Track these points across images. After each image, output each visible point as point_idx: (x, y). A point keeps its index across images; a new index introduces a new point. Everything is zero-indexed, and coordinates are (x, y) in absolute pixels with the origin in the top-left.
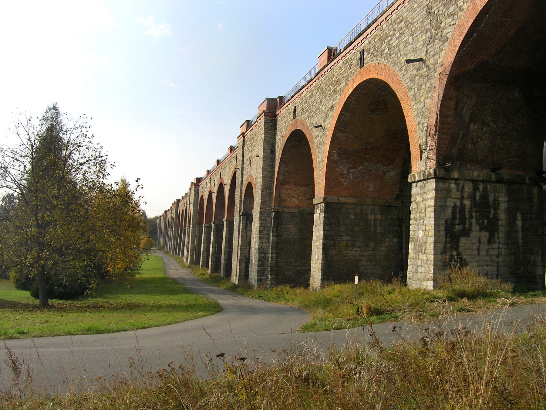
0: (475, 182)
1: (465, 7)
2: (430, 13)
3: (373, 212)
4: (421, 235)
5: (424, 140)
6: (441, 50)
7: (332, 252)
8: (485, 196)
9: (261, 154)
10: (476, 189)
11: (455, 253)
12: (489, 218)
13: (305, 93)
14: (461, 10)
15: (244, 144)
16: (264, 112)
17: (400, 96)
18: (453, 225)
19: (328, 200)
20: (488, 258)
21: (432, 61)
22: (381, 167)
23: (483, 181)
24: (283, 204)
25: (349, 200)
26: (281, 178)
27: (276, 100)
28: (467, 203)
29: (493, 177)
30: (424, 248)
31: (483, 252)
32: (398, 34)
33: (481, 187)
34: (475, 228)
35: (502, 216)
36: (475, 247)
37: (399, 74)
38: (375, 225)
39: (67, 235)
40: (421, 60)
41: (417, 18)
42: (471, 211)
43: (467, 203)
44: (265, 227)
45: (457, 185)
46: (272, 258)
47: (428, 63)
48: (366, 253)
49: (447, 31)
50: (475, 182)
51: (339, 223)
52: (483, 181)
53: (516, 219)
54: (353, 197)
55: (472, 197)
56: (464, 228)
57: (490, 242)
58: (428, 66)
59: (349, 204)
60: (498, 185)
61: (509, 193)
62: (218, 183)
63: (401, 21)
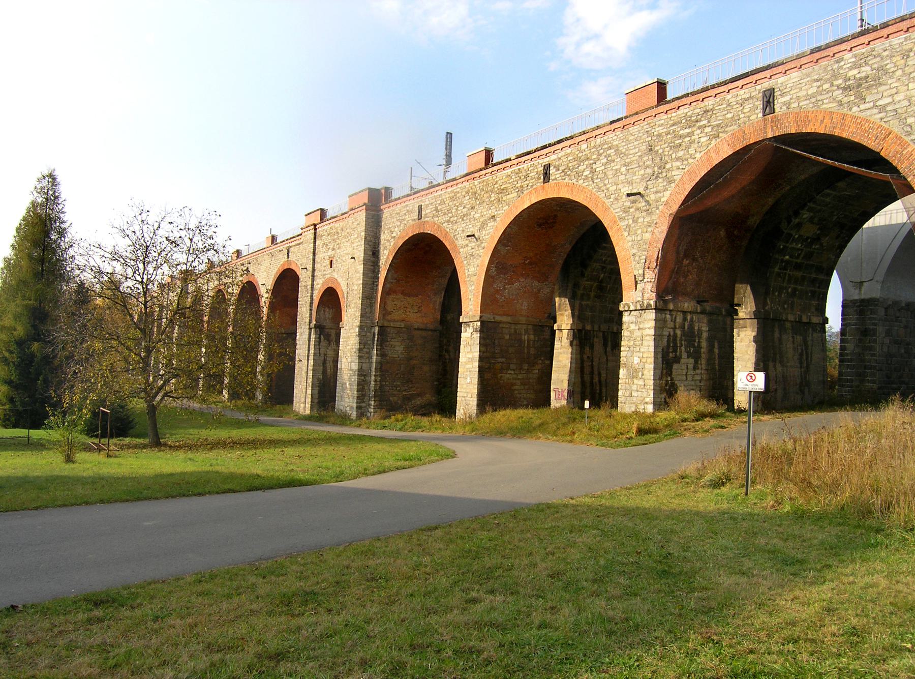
1: (698, 156)
2: (651, 150)
4: (636, 362)
5: (641, 272)
8: (691, 327)
10: (685, 319)
15: (315, 238)
16: (365, 204)
18: (668, 353)
19: (484, 319)
20: (693, 383)
21: (653, 197)
22: (536, 283)
23: (690, 312)
24: (389, 317)
25: (505, 319)
26: (388, 286)
27: (378, 190)
28: (679, 332)
30: (640, 374)
31: (689, 378)
32: (605, 160)
34: (684, 355)
35: (704, 344)
37: (607, 201)
40: (639, 194)
41: (634, 151)
42: (681, 340)
43: (679, 332)
44: (365, 344)
45: (671, 315)
46: (375, 381)
47: (647, 199)
49: (674, 173)
50: (684, 313)
51: (494, 343)
54: (507, 315)
57: (695, 368)
58: (647, 201)
59: (504, 323)
60: (702, 316)
61: (710, 322)
63: (610, 148)
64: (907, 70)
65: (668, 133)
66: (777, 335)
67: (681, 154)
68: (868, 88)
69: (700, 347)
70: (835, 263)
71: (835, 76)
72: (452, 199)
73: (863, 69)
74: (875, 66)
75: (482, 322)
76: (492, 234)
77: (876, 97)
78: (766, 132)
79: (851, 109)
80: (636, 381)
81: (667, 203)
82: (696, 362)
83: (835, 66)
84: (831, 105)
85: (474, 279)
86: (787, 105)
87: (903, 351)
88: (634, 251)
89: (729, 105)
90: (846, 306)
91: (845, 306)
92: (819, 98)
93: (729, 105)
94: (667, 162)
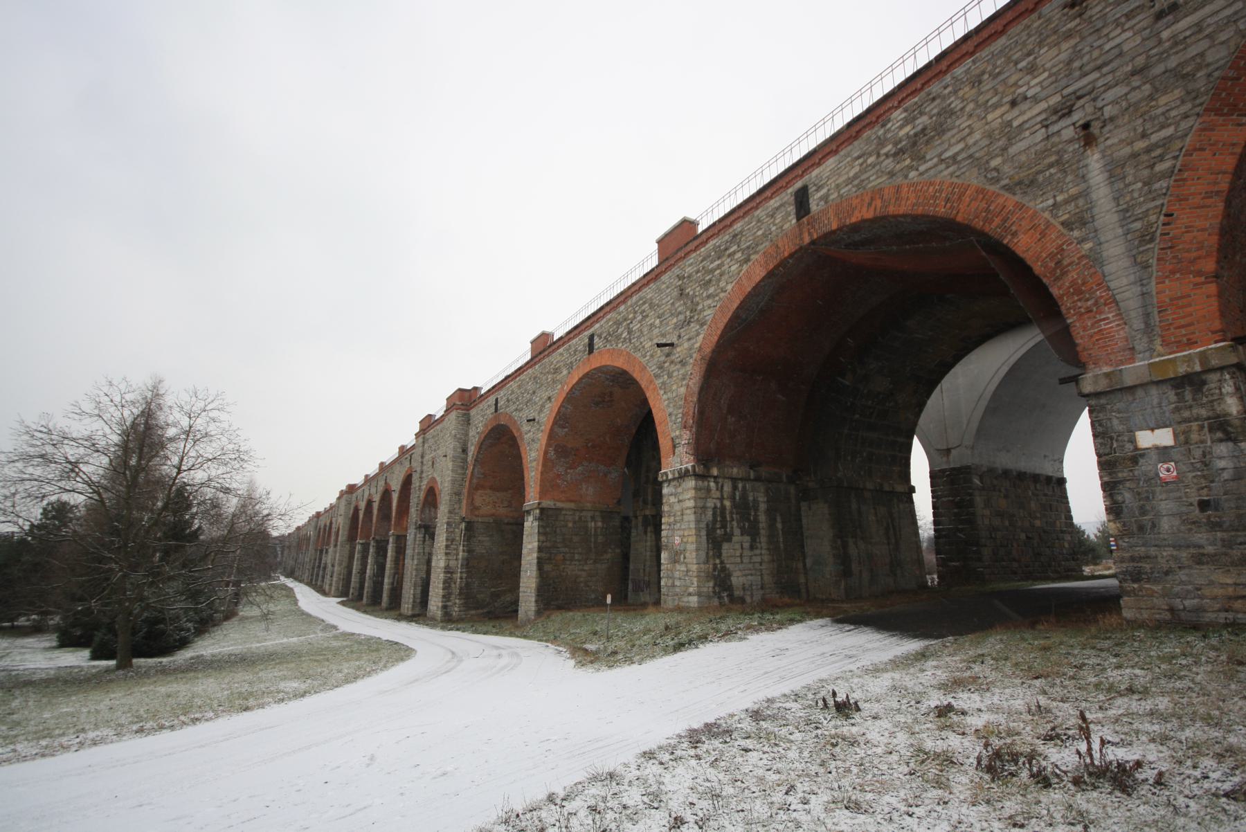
0: (734, 480)
1: (729, 287)
3: (593, 518)
6: (698, 334)
7: (547, 567)
8: (744, 496)
9: (450, 453)
10: (735, 488)
11: (718, 561)
12: (749, 520)
13: (513, 385)
14: (723, 290)
17: (643, 384)
18: (714, 529)
20: (750, 566)
22: (602, 467)
23: (741, 479)
28: (727, 503)
29: (752, 476)
31: (746, 560)
33: (740, 485)
34: (737, 531)
35: (762, 517)
36: (738, 553)
38: (596, 535)
39: (126, 574)
40: (672, 345)
42: (731, 513)
43: (727, 503)
45: (717, 483)
48: (586, 568)
50: (734, 480)
52: (741, 479)
53: (775, 520)
54: (571, 501)
55: (732, 498)
56: (726, 533)
57: (752, 548)
60: (758, 484)
62: (381, 489)
63: (644, 303)
64: (982, 99)
65: (698, 272)
66: (854, 506)
67: (711, 290)
68: (927, 142)
69: (756, 521)
70: (915, 424)
71: (882, 142)
72: (519, 387)
73: (917, 122)
74: (935, 111)
75: (542, 510)
76: (546, 417)
77: (939, 150)
78: (802, 239)
79: (906, 177)
80: (678, 566)
81: (700, 349)
82: (753, 540)
83: (881, 132)
84: (880, 180)
85: (534, 464)
86: (825, 198)
87: (1007, 523)
88: (670, 410)
89: (759, 221)
90: (935, 477)
91: (934, 476)
92: (863, 177)
93: (759, 221)
94: (698, 304)
